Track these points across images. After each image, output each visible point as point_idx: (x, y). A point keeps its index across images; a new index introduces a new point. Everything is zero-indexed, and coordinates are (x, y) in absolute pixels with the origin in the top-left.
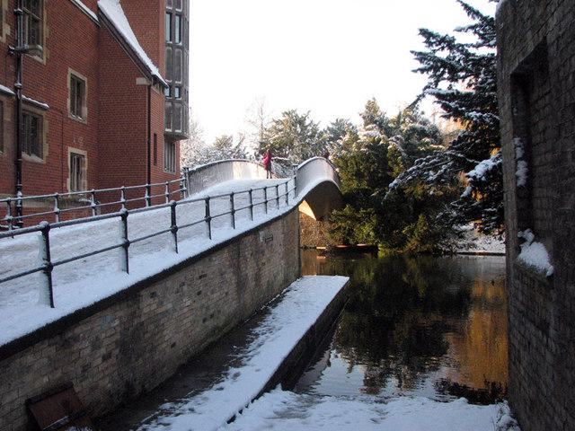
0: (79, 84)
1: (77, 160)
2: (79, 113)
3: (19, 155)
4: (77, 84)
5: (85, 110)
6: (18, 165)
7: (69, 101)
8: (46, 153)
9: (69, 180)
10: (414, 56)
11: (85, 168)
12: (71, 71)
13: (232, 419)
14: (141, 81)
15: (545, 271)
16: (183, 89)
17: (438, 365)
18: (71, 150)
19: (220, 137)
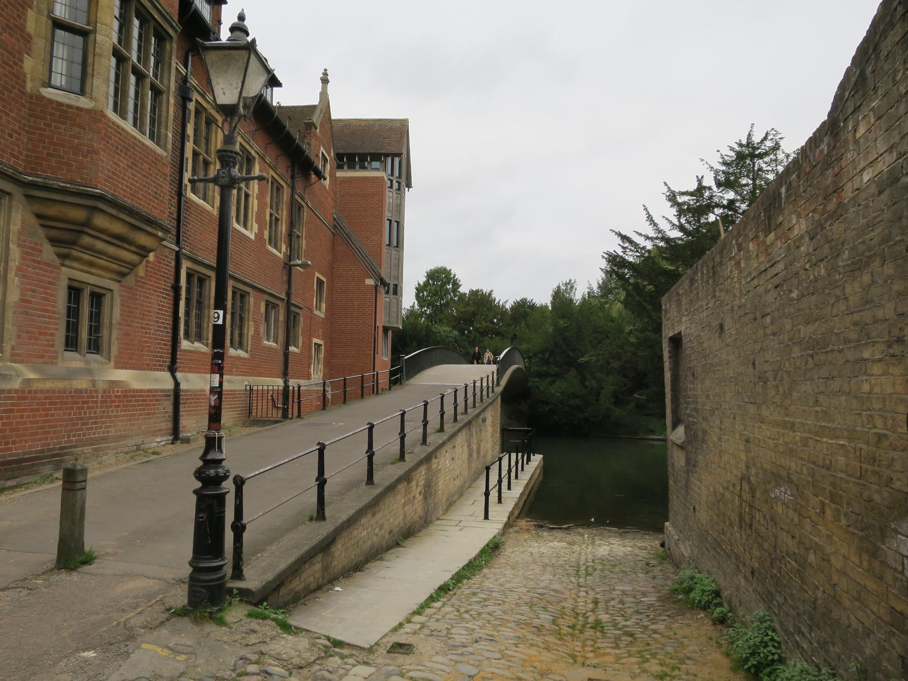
0: (320, 283)
1: (318, 346)
2: (320, 310)
3: (287, 349)
4: (320, 282)
5: (324, 306)
6: (286, 355)
7: (315, 299)
8: (300, 344)
9: (312, 366)
10: (665, 189)
11: (322, 356)
12: (317, 274)
13: (325, 81)
14: (370, 282)
15: (534, 455)
16: (400, 224)
17: (625, 376)
18: (315, 340)
19: (426, 275)
